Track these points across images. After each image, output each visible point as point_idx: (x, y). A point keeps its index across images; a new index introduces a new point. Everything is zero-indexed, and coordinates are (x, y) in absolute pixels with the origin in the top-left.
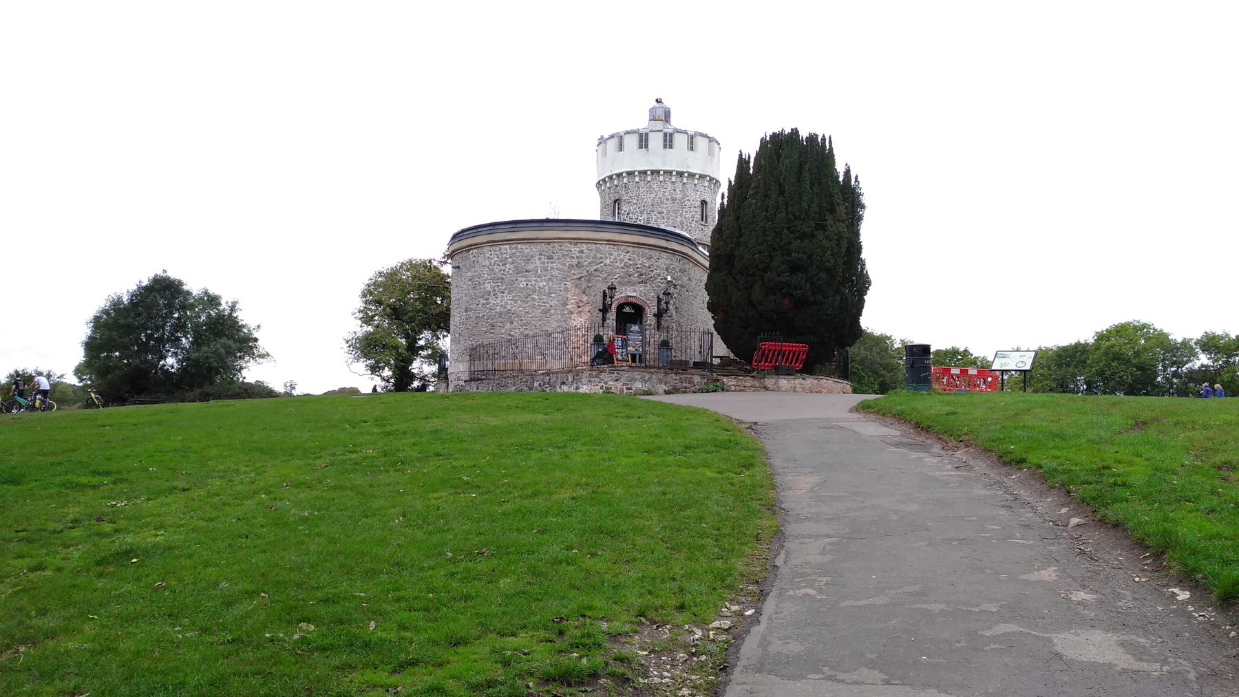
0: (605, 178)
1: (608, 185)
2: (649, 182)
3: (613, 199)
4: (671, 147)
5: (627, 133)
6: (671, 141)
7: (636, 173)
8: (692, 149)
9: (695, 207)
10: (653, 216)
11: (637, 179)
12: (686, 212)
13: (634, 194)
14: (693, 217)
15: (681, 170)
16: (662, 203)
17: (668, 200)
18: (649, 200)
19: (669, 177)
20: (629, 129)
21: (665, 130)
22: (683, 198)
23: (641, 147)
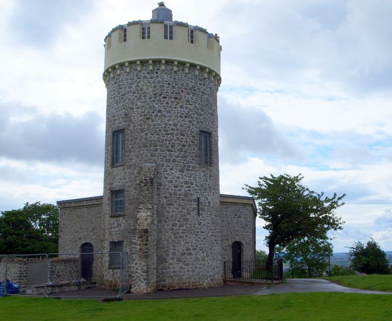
6: (171, 33)
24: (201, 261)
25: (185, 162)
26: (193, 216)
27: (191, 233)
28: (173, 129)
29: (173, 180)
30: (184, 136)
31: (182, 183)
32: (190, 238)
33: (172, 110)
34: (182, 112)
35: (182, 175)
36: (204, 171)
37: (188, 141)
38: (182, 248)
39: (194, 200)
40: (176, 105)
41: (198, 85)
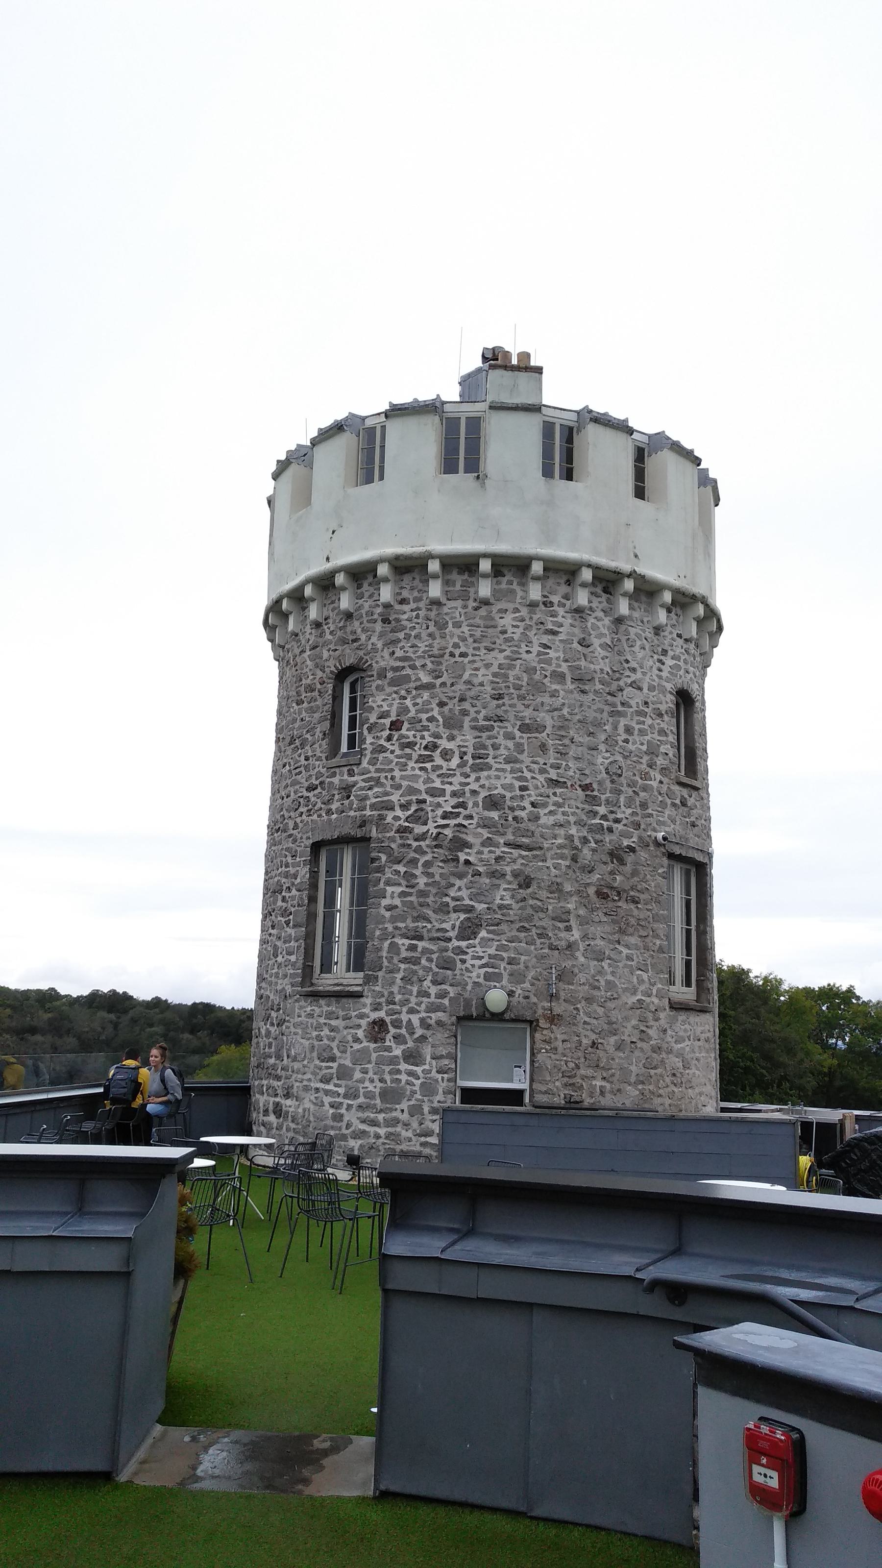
0: (300, 588)
1: (313, 612)
2: (486, 602)
3: (332, 666)
4: (569, 476)
5: (396, 411)
6: (569, 456)
7: (434, 566)
9: (660, 715)
10: (501, 740)
11: (435, 590)
12: (628, 730)
13: (422, 646)
14: (652, 751)
15: (612, 564)
16: (538, 688)
17: (559, 677)
18: (484, 676)
19: (564, 589)
20: (404, 398)
22: (616, 674)
23: (449, 466)
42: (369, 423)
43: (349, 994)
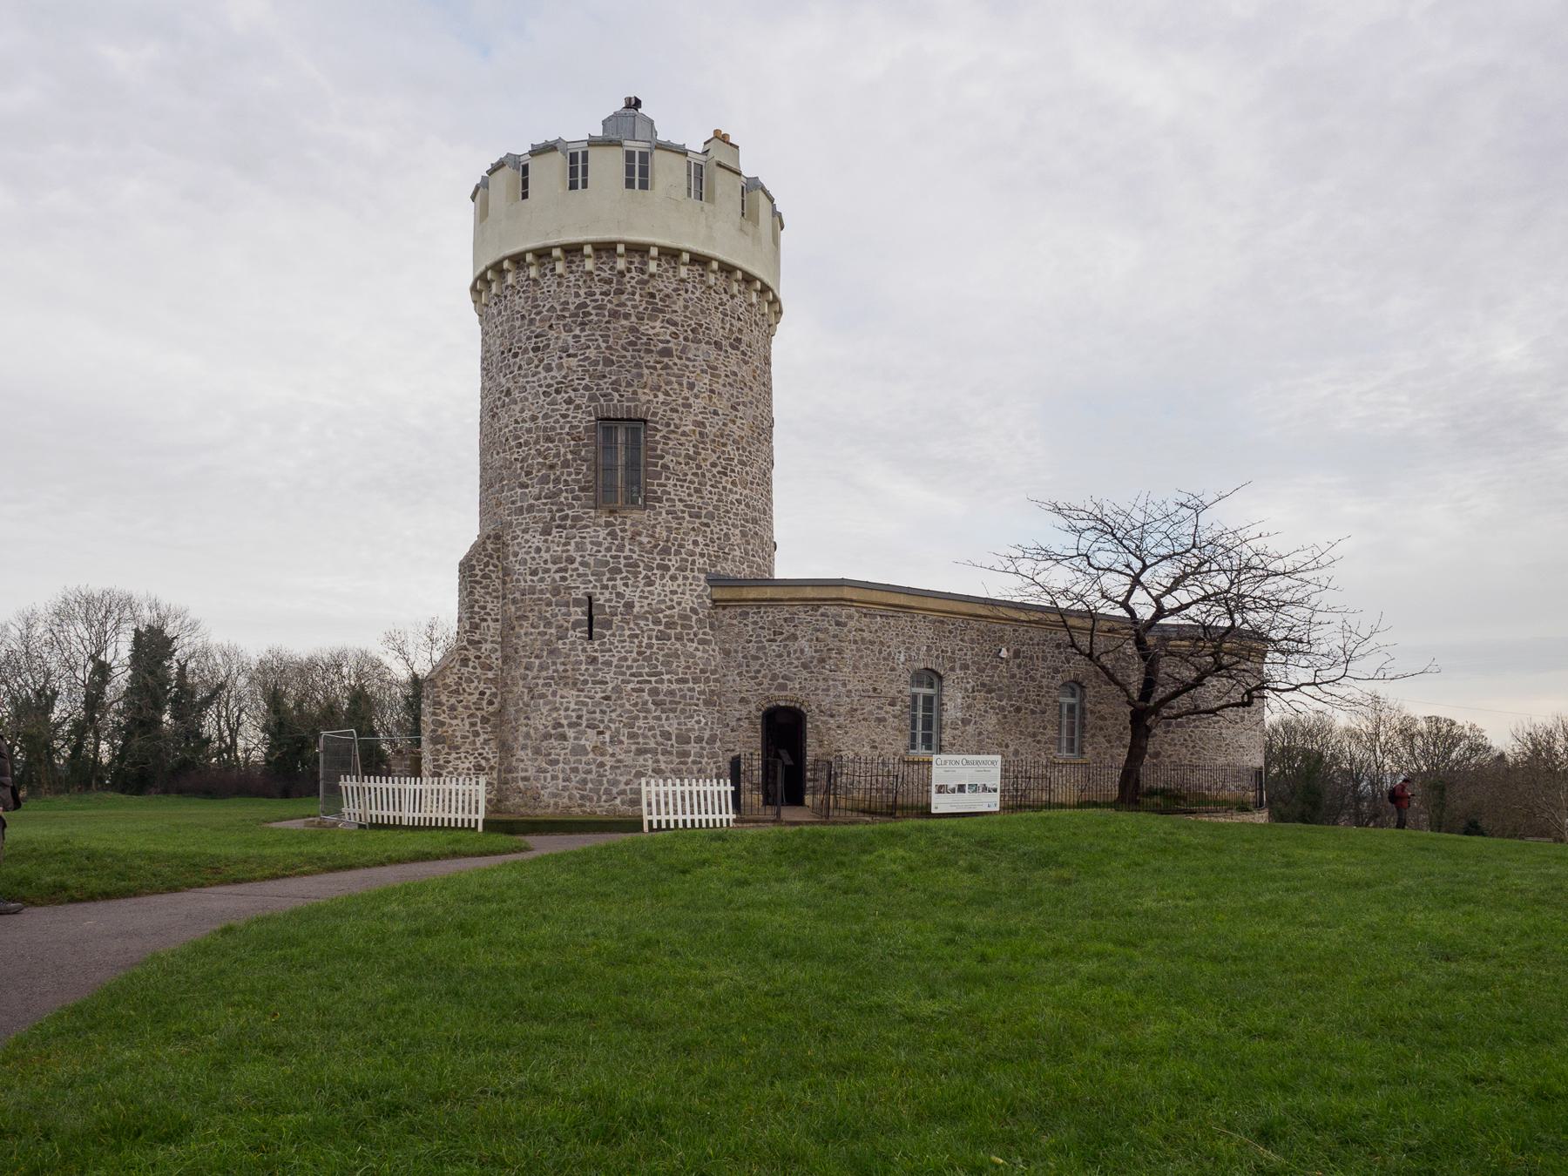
0: (500, 262)
4: (644, 185)
5: (537, 151)
6: (644, 172)
8: (525, 196)
21: (630, 145)
24: (591, 756)
25: (554, 508)
26: (573, 643)
27: (566, 684)
28: (529, 431)
29: (528, 557)
30: (552, 442)
31: (546, 562)
32: (562, 697)
33: (527, 382)
34: (549, 381)
35: (546, 541)
36: (608, 524)
37: (562, 450)
38: (543, 721)
39: (577, 602)
40: (537, 367)
41: (598, 297)
42: (572, 148)
43: (441, 841)
